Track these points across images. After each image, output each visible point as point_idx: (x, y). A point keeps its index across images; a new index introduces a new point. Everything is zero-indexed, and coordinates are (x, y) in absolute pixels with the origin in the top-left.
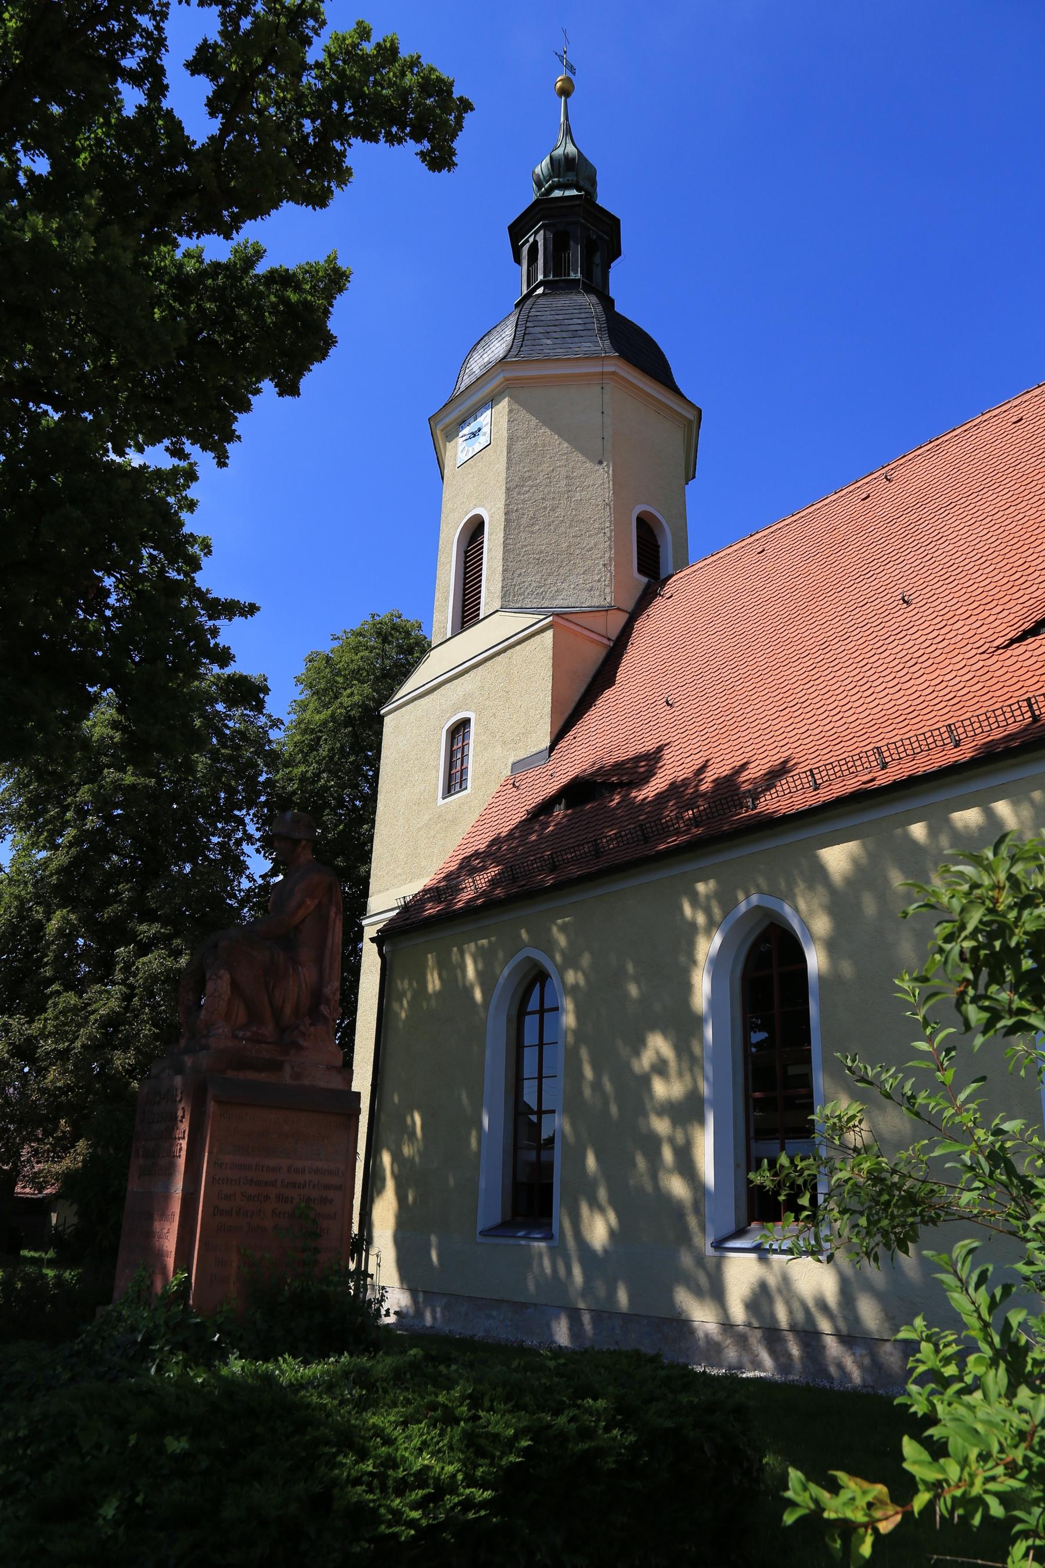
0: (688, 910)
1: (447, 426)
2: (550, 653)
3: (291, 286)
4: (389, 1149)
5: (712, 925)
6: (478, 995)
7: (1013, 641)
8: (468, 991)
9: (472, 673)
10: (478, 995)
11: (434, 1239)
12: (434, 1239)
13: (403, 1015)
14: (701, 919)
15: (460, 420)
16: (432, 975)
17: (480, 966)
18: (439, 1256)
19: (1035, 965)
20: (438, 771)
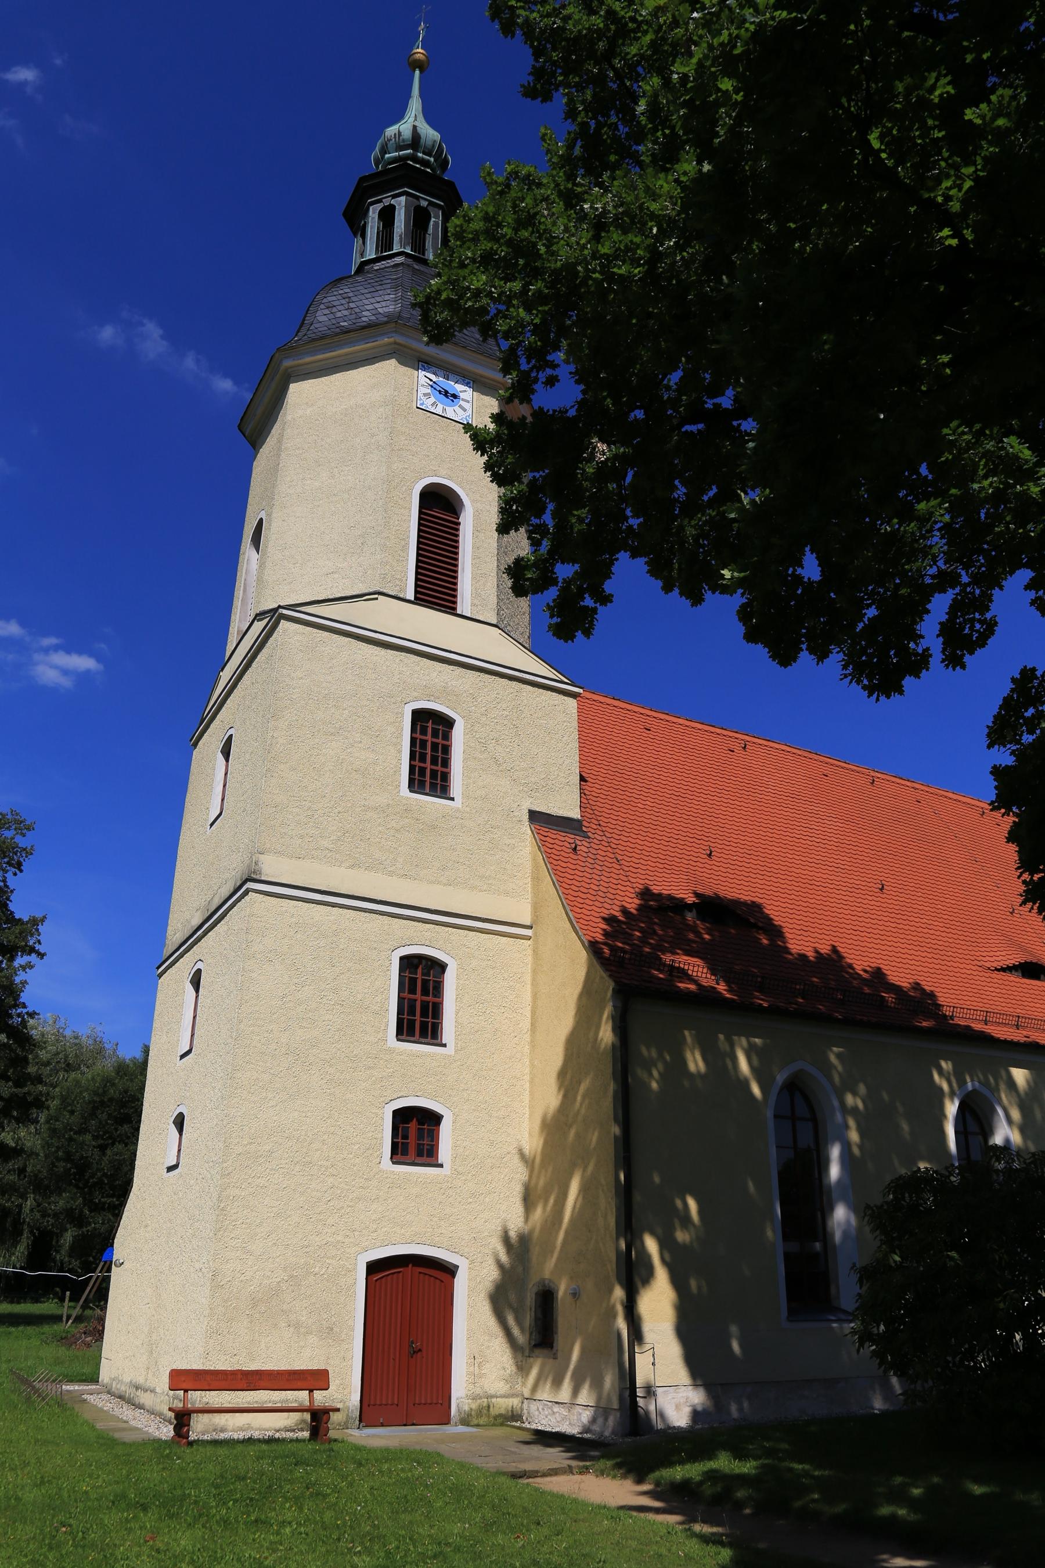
0: (936, 1077)
1: (405, 346)
2: (575, 724)
3: (567, 40)
4: (653, 1233)
5: (952, 1094)
6: (756, 1090)
7: (1003, 970)
8: (745, 1085)
9: (459, 671)
10: (756, 1090)
11: (734, 1329)
12: (734, 1329)
13: (654, 1085)
14: (945, 1086)
15: (428, 359)
16: (693, 1054)
17: (756, 1062)
18: (741, 1346)
19: (991, 1143)
20: (400, 751)
